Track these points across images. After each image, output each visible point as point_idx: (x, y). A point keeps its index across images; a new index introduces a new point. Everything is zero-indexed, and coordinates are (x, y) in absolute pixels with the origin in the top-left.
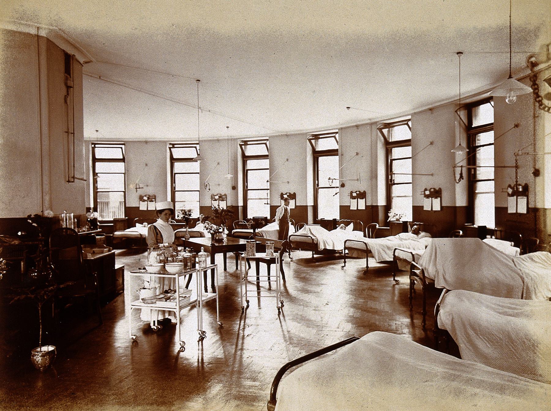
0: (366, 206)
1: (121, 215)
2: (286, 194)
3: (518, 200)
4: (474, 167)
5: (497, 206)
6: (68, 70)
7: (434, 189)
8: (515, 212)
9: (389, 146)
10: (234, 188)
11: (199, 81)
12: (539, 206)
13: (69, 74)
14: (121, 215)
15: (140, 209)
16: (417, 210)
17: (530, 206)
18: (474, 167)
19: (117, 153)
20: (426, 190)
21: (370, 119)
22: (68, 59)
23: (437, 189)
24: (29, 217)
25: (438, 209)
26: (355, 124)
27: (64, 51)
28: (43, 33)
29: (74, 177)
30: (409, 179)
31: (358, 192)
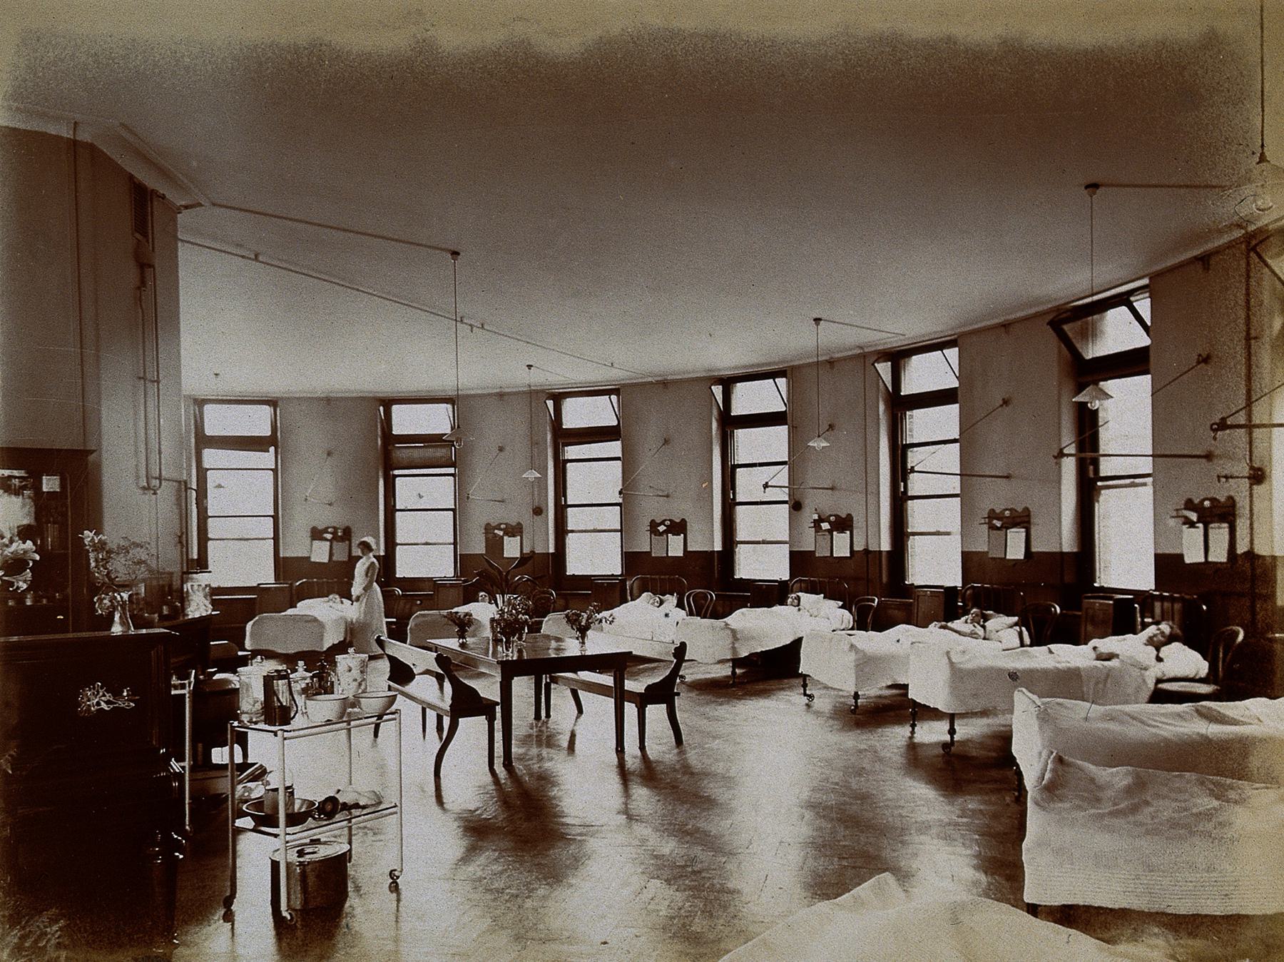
0: (852, 551)
1: (265, 575)
2: (663, 523)
3: (1211, 532)
4: (1083, 455)
5: (1159, 551)
6: (142, 224)
7: (1213, 500)
8: (1203, 560)
9: (900, 404)
10: (538, 511)
11: (458, 254)
12: (1261, 549)
13: (145, 235)
14: (265, 575)
15: (1188, 560)
16: (1168, 566)
17: (856, 548)
18: (1083, 455)
19: (258, 422)
20: (821, 520)
21: (861, 348)
22: (142, 198)
23: (1020, 510)
24: (1018, 766)
25: (1222, 558)
26: (1001, 320)
27: (131, 177)
28: (84, 136)
29: (160, 478)
30: (954, 485)
31: (668, 523)
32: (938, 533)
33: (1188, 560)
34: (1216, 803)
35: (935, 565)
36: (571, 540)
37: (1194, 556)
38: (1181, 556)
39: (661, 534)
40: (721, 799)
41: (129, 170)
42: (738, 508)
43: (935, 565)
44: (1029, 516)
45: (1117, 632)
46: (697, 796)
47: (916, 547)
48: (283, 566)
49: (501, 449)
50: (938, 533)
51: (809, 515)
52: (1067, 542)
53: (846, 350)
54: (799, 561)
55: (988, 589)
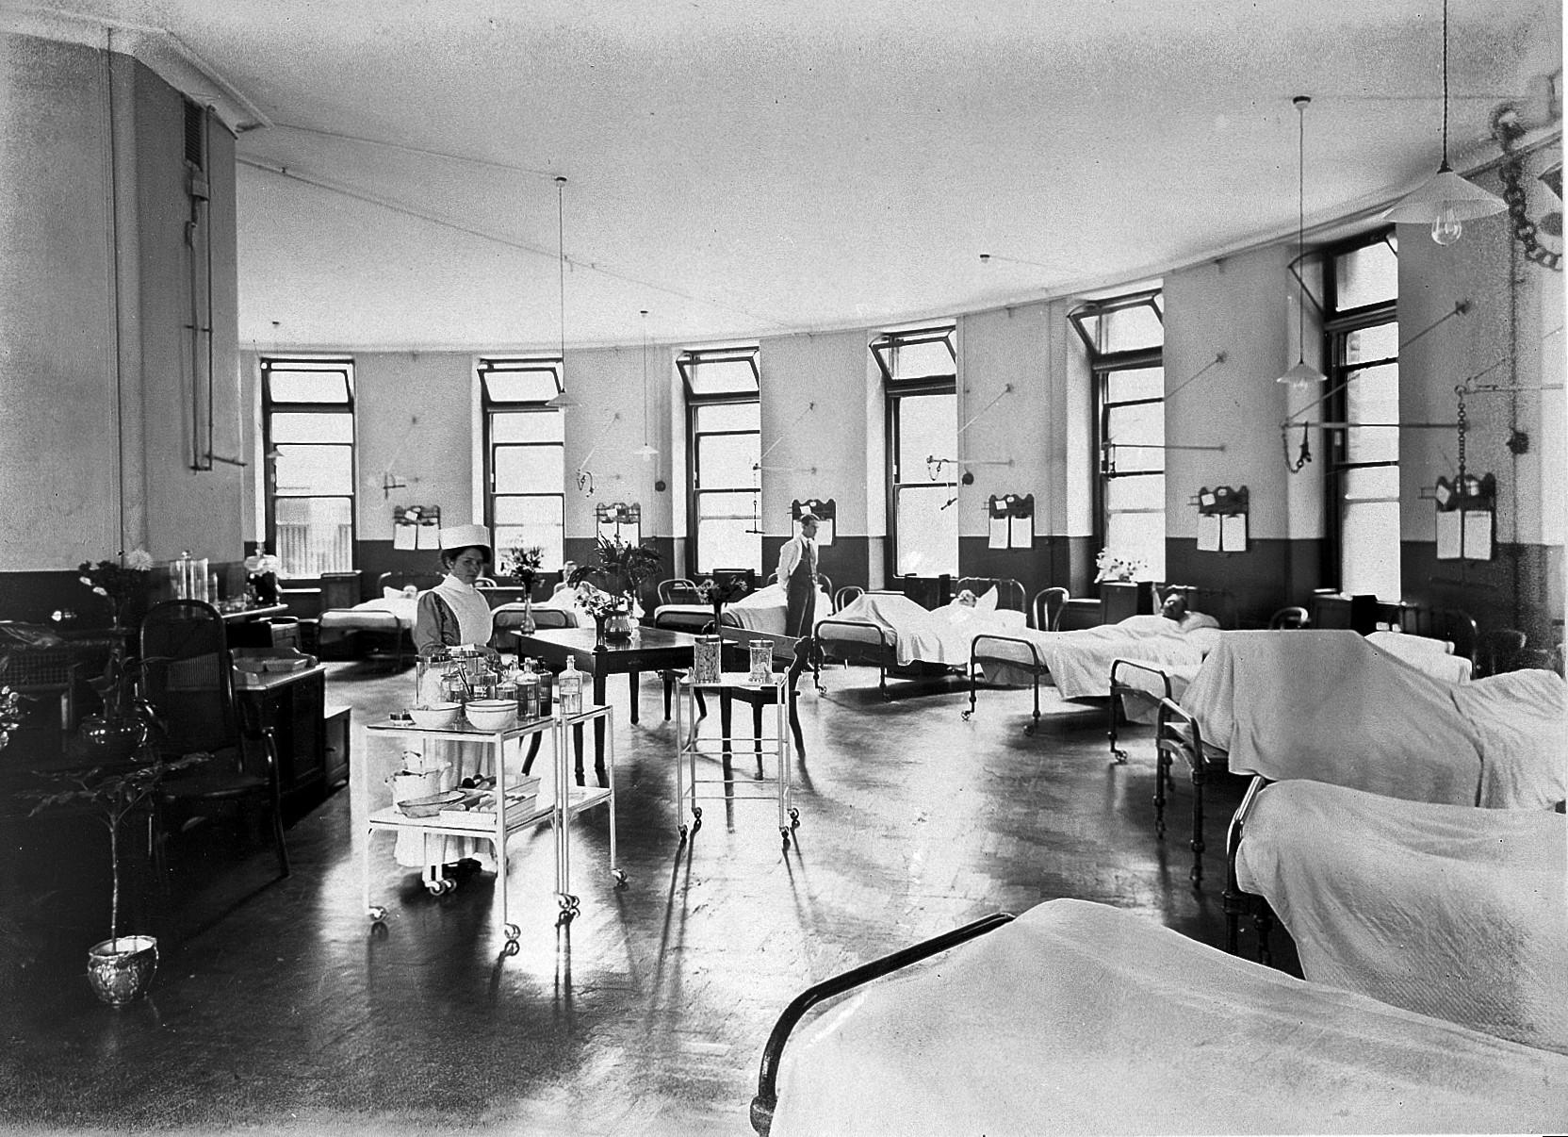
5: (1412, 538)
10: (661, 486)
12: (1526, 538)
15: (1200, 548)
16: (1179, 551)
20: (1204, 491)
27: (182, 95)
28: (124, 45)
29: (209, 456)
31: (1011, 500)
32: (1145, 511)
33: (1200, 548)
34: (860, 771)
35: (1136, 553)
36: (702, 526)
37: (1207, 544)
38: (1433, 546)
39: (407, 523)
40: (992, 836)
41: (180, 88)
42: (1396, 459)
43: (1136, 553)
44: (1494, 482)
45: (364, 600)
46: (1021, 838)
47: (1117, 528)
48: (363, 551)
49: (1221, 359)
50: (1145, 511)
51: (980, 492)
52: (1305, 524)
53: (1258, 233)
54: (972, 549)
55: (1201, 586)
